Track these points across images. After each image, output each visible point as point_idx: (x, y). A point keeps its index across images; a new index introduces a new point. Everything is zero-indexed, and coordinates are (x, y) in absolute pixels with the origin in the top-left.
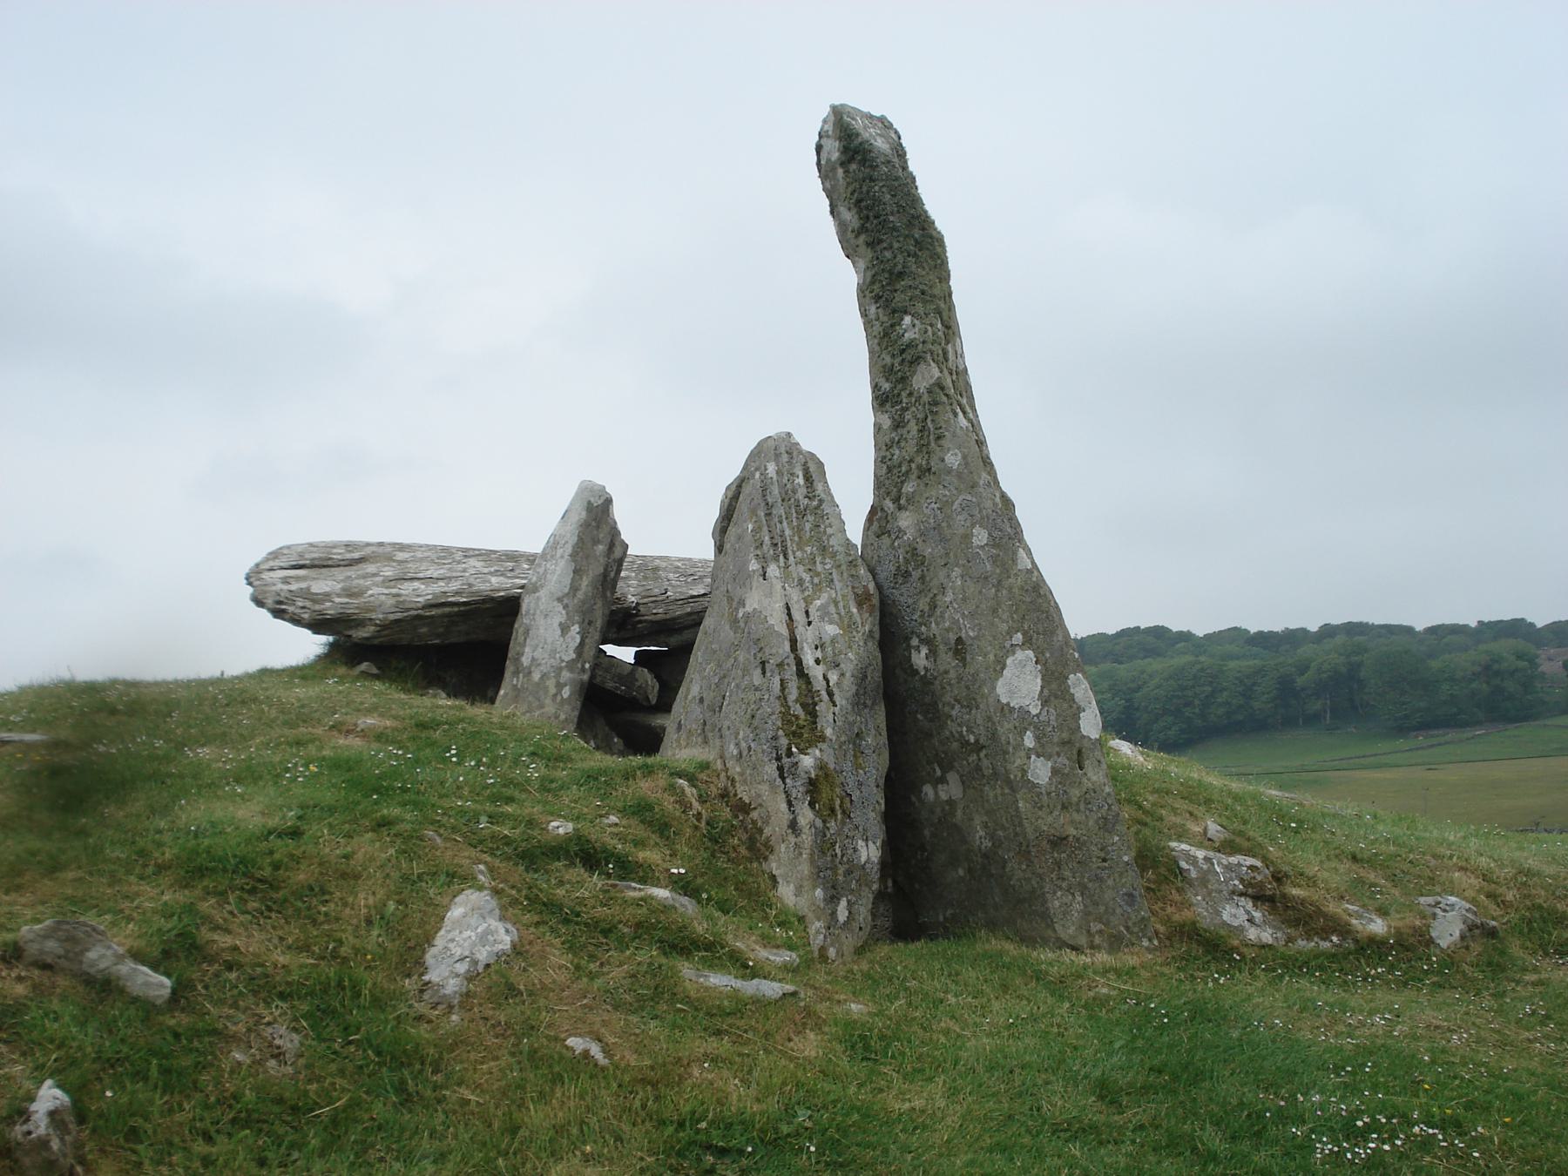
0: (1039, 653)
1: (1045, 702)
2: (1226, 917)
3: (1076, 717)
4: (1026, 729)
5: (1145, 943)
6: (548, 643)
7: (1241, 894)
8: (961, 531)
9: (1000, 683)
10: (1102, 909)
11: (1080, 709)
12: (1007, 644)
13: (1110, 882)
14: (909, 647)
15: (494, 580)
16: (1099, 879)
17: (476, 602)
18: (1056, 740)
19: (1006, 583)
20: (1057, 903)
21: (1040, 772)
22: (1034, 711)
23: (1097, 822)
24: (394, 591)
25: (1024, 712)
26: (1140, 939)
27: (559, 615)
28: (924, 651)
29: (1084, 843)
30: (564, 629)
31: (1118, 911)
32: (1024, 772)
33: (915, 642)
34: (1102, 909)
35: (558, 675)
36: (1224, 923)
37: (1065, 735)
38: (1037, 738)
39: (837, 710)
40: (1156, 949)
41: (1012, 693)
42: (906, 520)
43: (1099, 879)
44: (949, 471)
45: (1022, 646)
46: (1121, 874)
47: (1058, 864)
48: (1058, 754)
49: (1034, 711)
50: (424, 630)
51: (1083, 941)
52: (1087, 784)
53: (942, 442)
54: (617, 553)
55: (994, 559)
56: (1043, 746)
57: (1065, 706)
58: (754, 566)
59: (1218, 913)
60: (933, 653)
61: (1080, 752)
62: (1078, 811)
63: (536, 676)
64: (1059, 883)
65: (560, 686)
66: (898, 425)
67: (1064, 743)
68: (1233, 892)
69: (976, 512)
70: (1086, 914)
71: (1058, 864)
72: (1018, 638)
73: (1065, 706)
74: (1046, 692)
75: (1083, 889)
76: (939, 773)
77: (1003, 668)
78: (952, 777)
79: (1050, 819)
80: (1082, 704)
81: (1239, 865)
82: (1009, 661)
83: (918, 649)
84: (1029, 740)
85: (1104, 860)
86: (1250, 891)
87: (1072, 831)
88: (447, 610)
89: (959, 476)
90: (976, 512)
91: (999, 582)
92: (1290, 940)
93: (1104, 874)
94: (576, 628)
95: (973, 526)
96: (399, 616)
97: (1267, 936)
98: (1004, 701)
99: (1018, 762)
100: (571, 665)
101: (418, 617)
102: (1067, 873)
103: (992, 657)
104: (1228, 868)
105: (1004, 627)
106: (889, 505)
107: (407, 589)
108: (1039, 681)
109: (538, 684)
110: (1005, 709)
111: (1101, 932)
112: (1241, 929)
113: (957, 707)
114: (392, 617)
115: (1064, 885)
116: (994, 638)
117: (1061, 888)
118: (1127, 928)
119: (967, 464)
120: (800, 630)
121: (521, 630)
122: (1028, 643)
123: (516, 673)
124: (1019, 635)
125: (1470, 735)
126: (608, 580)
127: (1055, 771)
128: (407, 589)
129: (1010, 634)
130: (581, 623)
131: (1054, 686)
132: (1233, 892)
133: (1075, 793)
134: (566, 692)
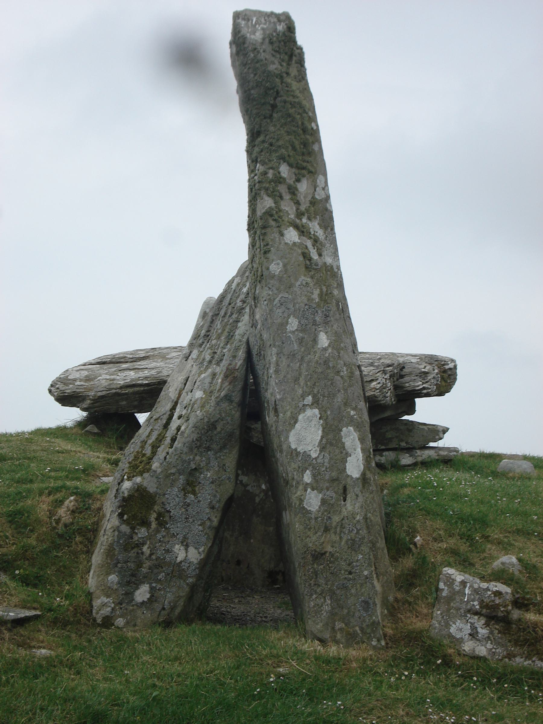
0: (323, 411)
1: (323, 448)
2: (453, 630)
3: (344, 461)
4: (307, 469)
5: (374, 643)
7: (476, 613)
8: (279, 320)
9: (292, 433)
10: (345, 611)
11: (348, 455)
12: (301, 405)
13: (353, 591)
16: (344, 587)
17: (154, 384)
18: (327, 477)
19: (307, 359)
20: (312, 604)
21: (313, 501)
22: (314, 455)
23: (347, 542)
25: (306, 455)
26: (370, 639)
29: (336, 559)
31: (357, 614)
32: (301, 501)
34: (345, 611)
36: (450, 636)
37: (334, 474)
38: (314, 476)
39: (171, 450)
40: (382, 648)
41: (299, 441)
43: (344, 587)
44: (273, 277)
45: (311, 406)
46: (362, 585)
47: (316, 573)
48: (328, 489)
49: (314, 455)
50: (124, 403)
51: (327, 635)
52: (345, 513)
53: (268, 255)
55: (301, 341)
56: (317, 481)
57: (337, 451)
59: (448, 626)
61: (345, 489)
62: (335, 533)
64: (315, 588)
67: (333, 480)
68: (469, 611)
69: (291, 306)
70: (332, 614)
71: (316, 573)
72: (309, 399)
73: (337, 451)
74: (324, 440)
75: (332, 593)
77: (296, 422)
79: (314, 538)
80: (349, 451)
81: (488, 589)
82: (300, 417)
84: (307, 477)
85: (350, 573)
86: (484, 611)
87: (329, 549)
89: (280, 279)
90: (291, 306)
91: (302, 358)
92: (510, 656)
93: (349, 584)
95: (289, 317)
96: (104, 393)
97: (482, 651)
98: (293, 447)
99: (299, 493)
102: (322, 581)
103: (289, 414)
104: (476, 591)
105: (300, 391)
108: (320, 432)
110: (294, 453)
111: (341, 629)
112: (461, 641)
114: (100, 394)
115: (319, 590)
116: (293, 399)
117: (316, 593)
118: (362, 629)
119: (286, 271)
122: (316, 403)
124: (310, 398)
127: (324, 502)
129: (303, 397)
131: (330, 436)
132: (469, 611)
133: (336, 519)
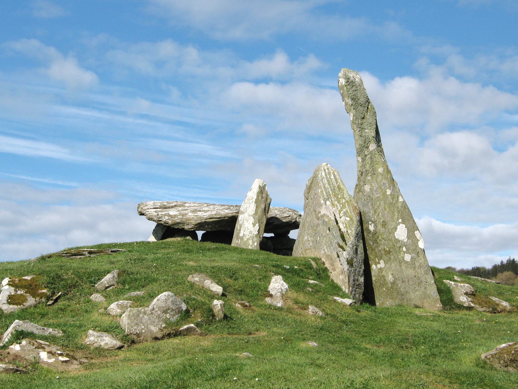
6: (248, 231)
14: (369, 224)
15: (226, 211)
24: (196, 214)
25: (402, 241)
27: (252, 220)
28: (373, 225)
30: (254, 225)
32: (403, 258)
33: (370, 223)
35: (253, 240)
42: (367, 188)
54: (268, 201)
58: (322, 202)
60: (376, 226)
63: (245, 239)
65: (253, 243)
66: (363, 160)
67: (413, 250)
72: (400, 221)
76: (377, 260)
78: (382, 262)
83: (371, 224)
84: (404, 249)
88: (215, 220)
94: (257, 224)
96: (199, 222)
100: (256, 236)
101: (205, 222)
106: (362, 184)
107: (200, 214)
109: (246, 242)
110: (398, 241)
113: (383, 241)
120: (338, 219)
121: (239, 226)
122: (403, 222)
123: (237, 239)
125: (172, 212)
126: (266, 210)
127: (412, 258)
128: (200, 214)
130: (259, 223)
134: (256, 244)
